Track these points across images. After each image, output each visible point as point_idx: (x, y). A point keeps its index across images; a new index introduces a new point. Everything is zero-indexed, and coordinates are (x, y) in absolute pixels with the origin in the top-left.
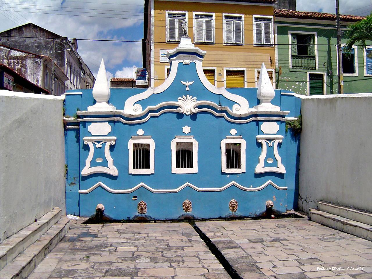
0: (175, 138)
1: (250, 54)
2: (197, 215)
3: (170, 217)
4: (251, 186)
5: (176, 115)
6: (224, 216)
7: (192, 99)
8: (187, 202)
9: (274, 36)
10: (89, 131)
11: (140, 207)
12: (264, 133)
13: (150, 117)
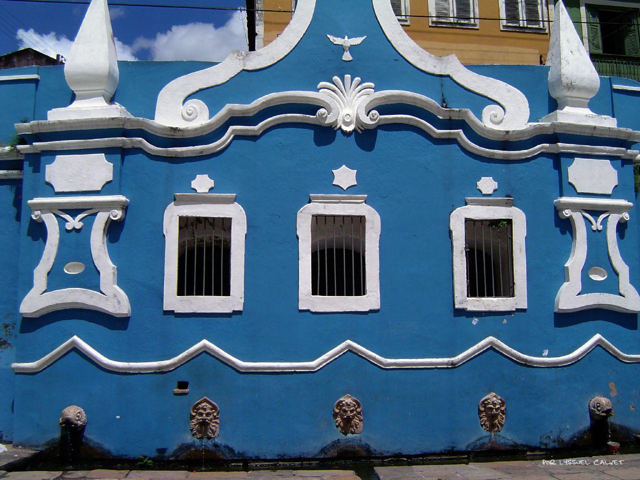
0: (310, 202)
1: (494, 48)
2: (379, 442)
3: (294, 450)
4: (546, 353)
5: (313, 131)
6: (462, 447)
7: (359, 87)
8: (349, 401)
9: (548, 9)
10: (47, 179)
11: (197, 417)
12: (578, 191)
13: (234, 139)
